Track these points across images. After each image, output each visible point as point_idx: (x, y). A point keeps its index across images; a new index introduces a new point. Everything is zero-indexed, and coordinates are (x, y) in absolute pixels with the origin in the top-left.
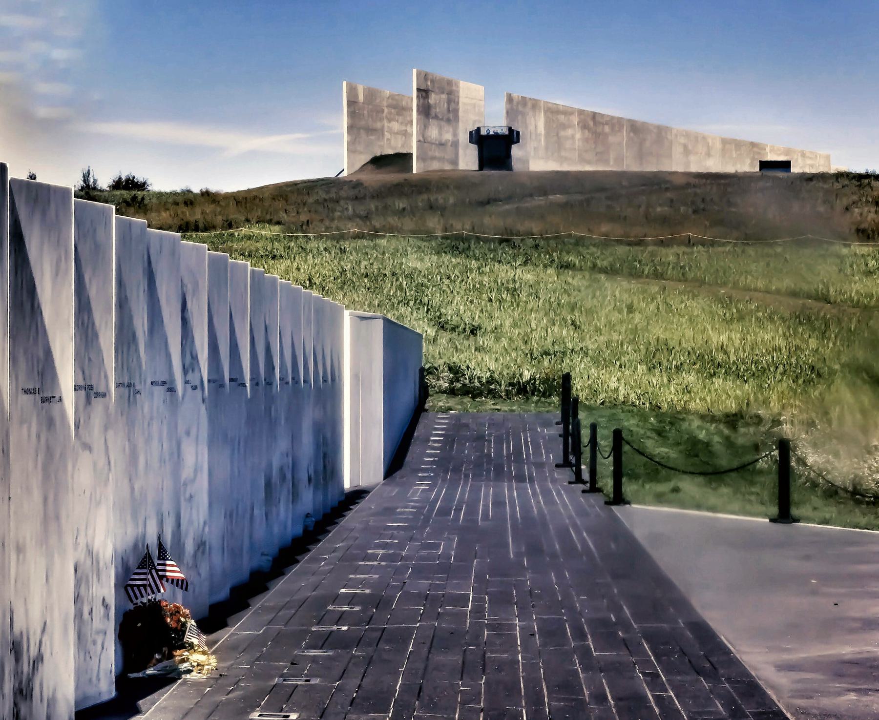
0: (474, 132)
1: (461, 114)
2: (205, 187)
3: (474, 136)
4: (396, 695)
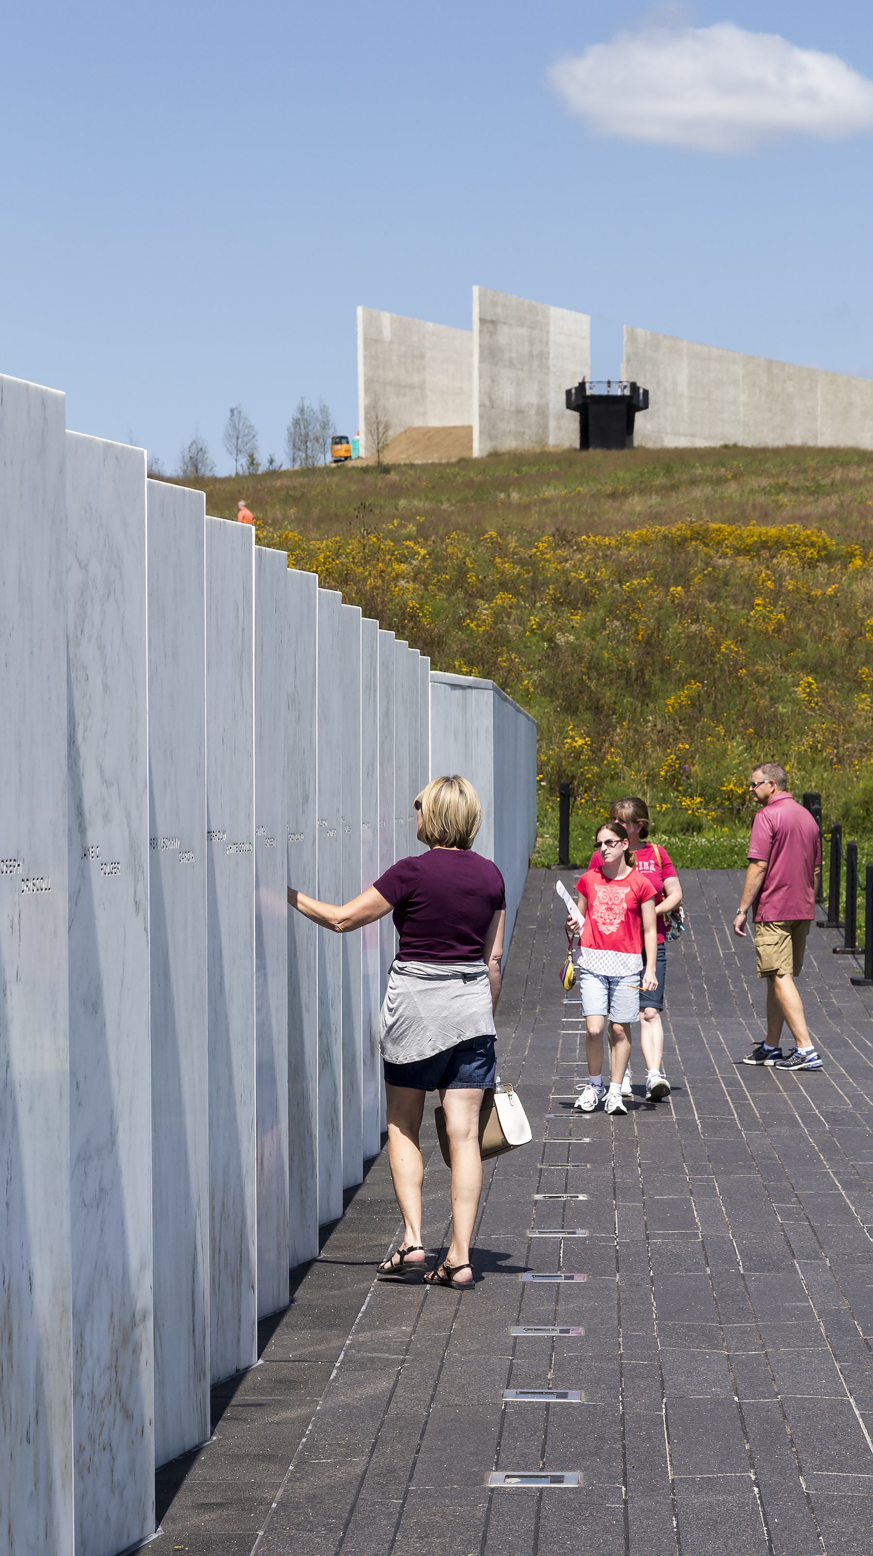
0: (573, 391)
1: (552, 362)
2: (625, 378)
3: (573, 398)
4: (635, 1127)
